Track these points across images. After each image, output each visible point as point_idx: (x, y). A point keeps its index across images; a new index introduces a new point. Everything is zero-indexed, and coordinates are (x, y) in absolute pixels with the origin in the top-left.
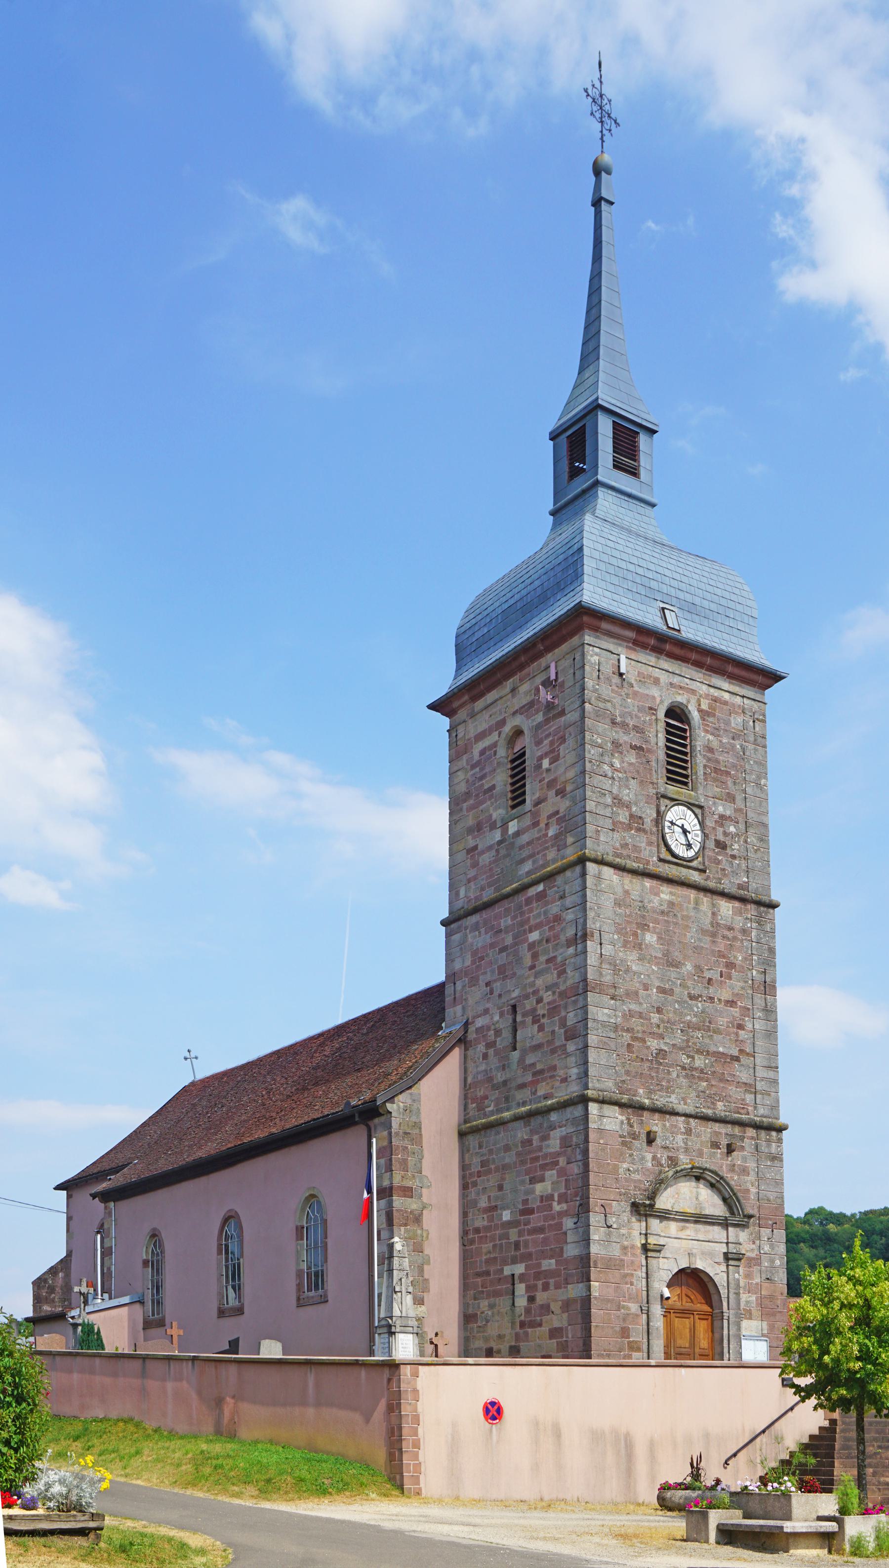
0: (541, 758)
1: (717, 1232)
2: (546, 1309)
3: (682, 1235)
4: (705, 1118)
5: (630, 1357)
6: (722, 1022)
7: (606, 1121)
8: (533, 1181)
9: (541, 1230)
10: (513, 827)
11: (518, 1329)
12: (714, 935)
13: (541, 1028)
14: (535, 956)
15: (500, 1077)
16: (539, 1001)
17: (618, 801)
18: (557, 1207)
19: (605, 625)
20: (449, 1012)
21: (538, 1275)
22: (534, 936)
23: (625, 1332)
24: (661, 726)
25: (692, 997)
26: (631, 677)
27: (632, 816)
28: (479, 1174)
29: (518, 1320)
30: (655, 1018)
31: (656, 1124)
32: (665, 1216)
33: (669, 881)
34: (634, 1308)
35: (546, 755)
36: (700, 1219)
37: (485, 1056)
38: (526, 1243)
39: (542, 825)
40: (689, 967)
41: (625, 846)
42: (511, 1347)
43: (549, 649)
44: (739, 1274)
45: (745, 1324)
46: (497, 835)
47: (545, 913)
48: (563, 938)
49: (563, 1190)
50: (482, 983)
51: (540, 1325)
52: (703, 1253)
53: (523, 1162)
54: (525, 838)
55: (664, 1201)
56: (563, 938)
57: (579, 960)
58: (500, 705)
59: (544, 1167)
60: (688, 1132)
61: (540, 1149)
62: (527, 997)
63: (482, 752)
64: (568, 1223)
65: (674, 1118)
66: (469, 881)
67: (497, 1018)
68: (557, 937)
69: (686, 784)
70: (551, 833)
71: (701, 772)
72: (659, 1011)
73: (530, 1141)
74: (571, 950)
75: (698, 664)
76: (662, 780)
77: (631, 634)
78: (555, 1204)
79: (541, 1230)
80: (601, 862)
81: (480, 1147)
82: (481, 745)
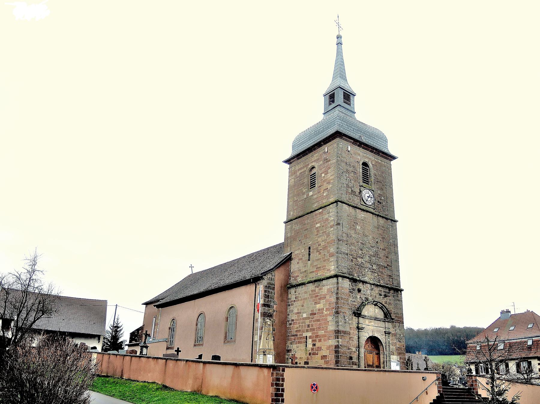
2: (320, 349)
3: (370, 324)
4: (377, 285)
5: (352, 367)
8: (316, 303)
9: (318, 320)
14: (318, 231)
15: (303, 270)
19: (344, 137)
22: (318, 225)
23: (351, 358)
26: (352, 152)
30: (360, 252)
31: (361, 286)
32: (364, 317)
34: (354, 349)
36: (376, 319)
37: (298, 263)
40: (371, 237)
42: (305, 362)
43: (325, 144)
45: (392, 356)
46: (305, 196)
48: (329, 226)
52: (377, 331)
54: (315, 196)
59: (320, 299)
60: (372, 289)
61: (319, 293)
62: (315, 244)
63: (300, 174)
68: (326, 225)
71: (373, 181)
73: (315, 290)
74: (332, 229)
78: (324, 311)
79: (318, 320)
82: (300, 172)
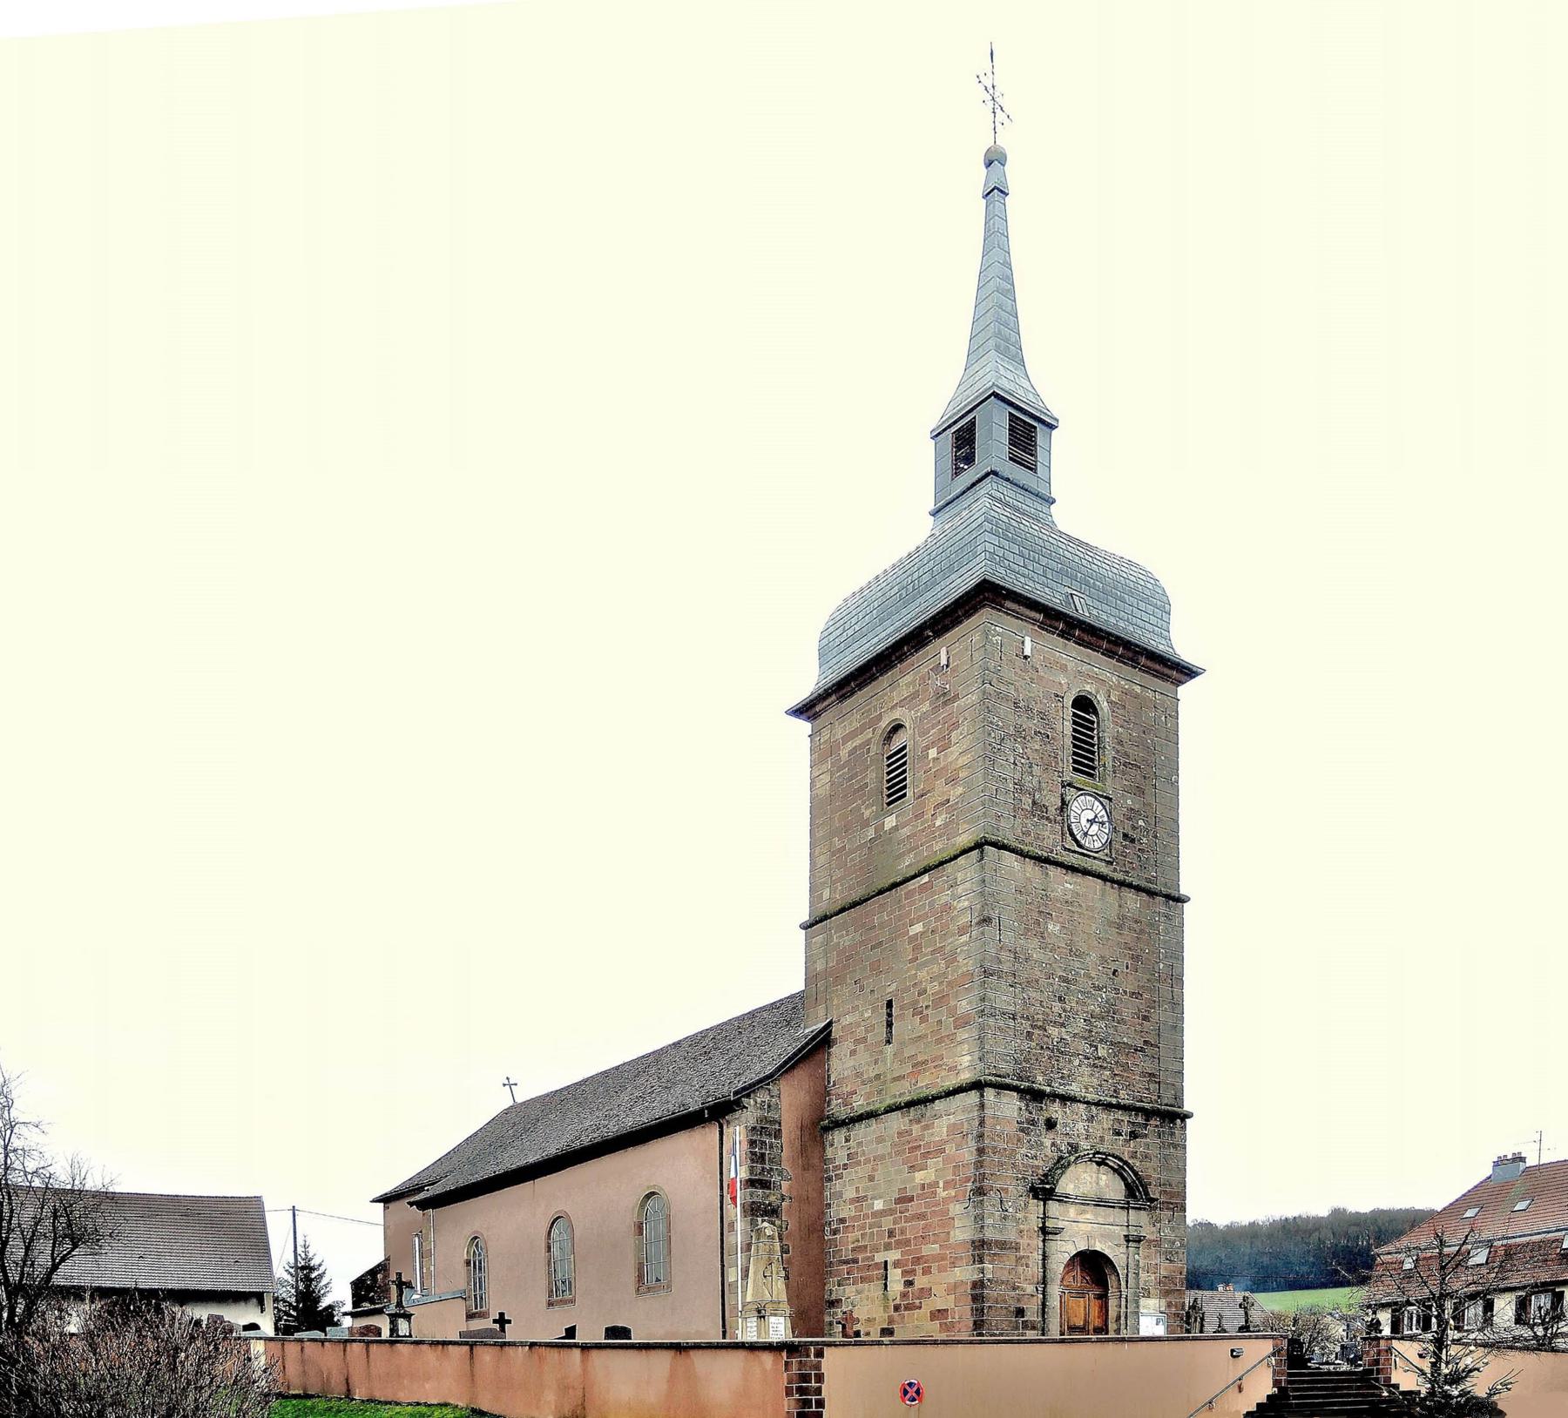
0: (927, 748)
1: (1119, 1216)
2: (926, 1292)
8: (913, 1168)
9: (922, 1216)
10: (890, 822)
12: (1120, 927)
13: (924, 1019)
14: (917, 948)
16: (922, 992)
21: (917, 1260)
22: (918, 928)
23: (1020, 1312)
24: (1070, 718)
26: (1037, 661)
27: (1034, 803)
28: (845, 1166)
29: (892, 1304)
30: (1057, 1007)
31: (1055, 1110)
32: (1063, 1199)
33: (1073, 869)
34: (1030, 1289)
36: (1100, 1203)
37: (853, 1053)
38: (903, 1232)
41: (1027, 833)
44: (1143, 1256)
45: (1143, 1301)
46: (871, 833)
47: (931, 904)
54: (906, 831)
55: (1066, 1185)
56: (953, 928)
60: (1091, 1119)
61: (921, 1138)
62: (907, 990)
65: (1075, 1105)
69: (1091, 775)
72: (1061, 999)
73: (909, 1132)
74: (965, 938)
76: (1068, 766)
79: (922, 1216)
81: (847, 1140)
82: (850, 745)
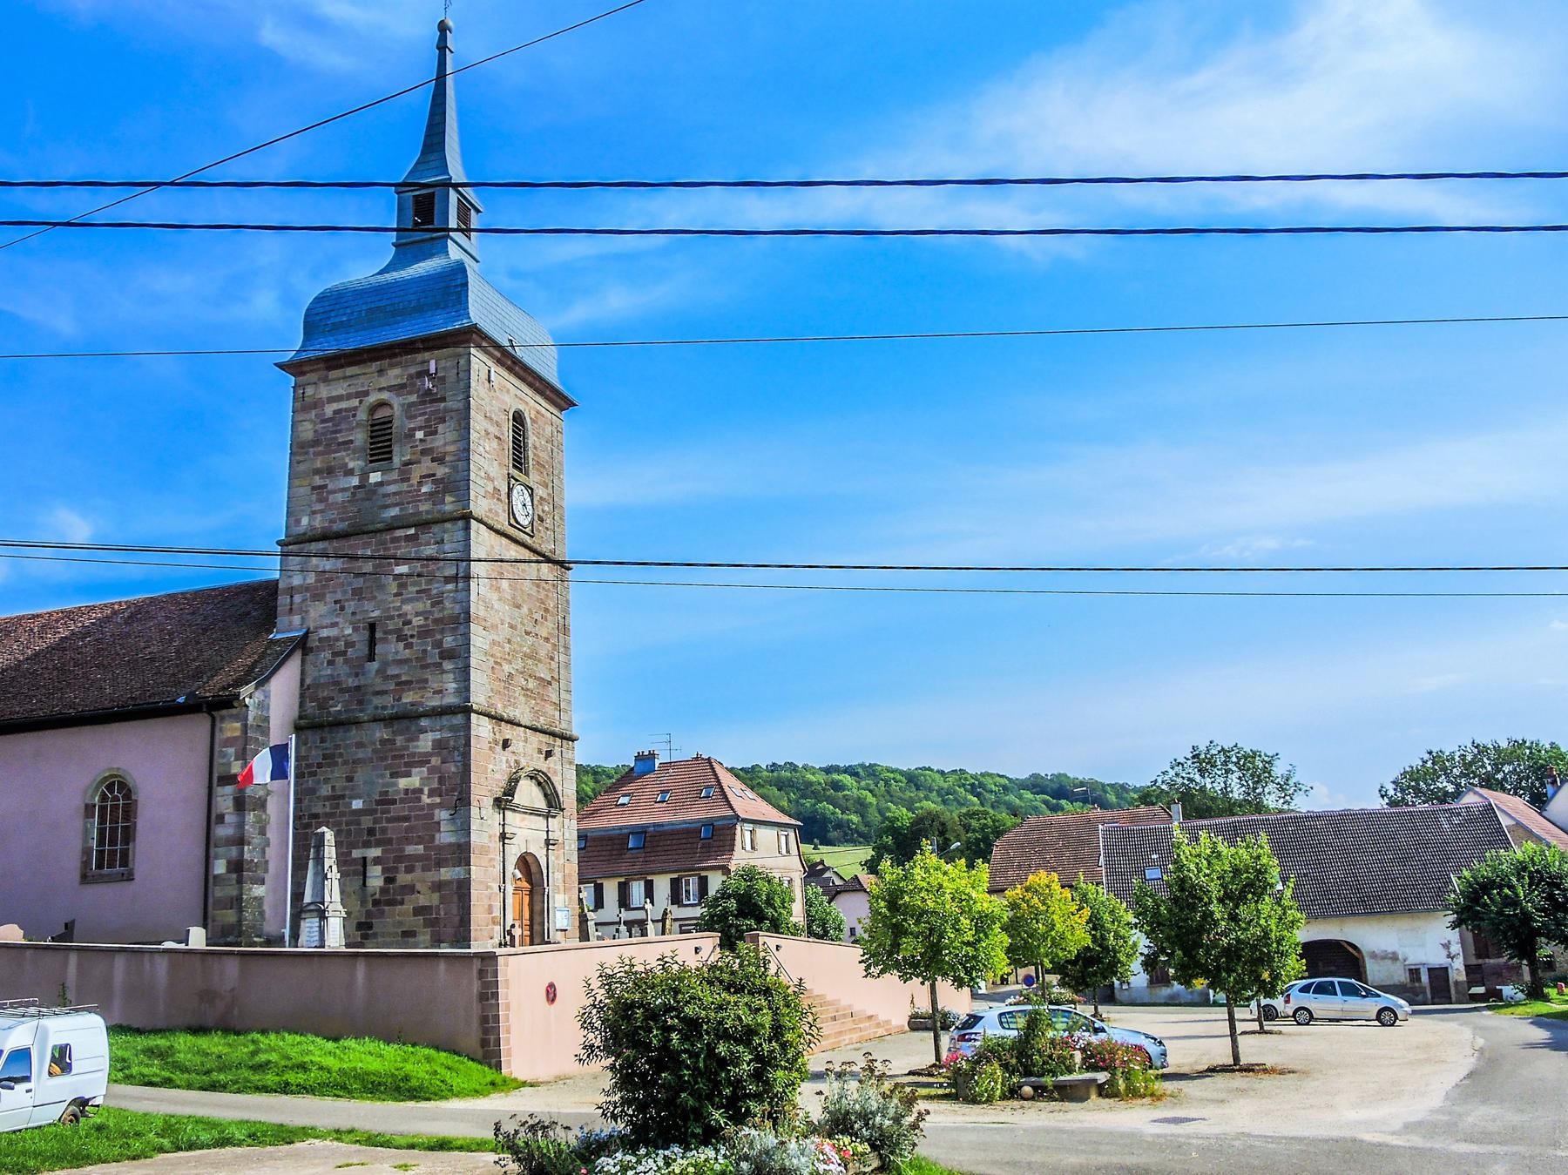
6: (542, 653)
7: (481, 729)
9: (406, 819)
11: (370, 906)
17: (488, 478)
18: (426, 800)
20: (282, 621)
25: (527, 633)
28: (320, 766)
31: (508, 732)
35: (420, 429)
37: (331, 663)
39: (414, 481)
46: (355, 481)
49: (436, 785)
50: (329, 598)
51: (402, 903)
53: (383, 759)
57: (460, 596)
58: (362, 379)
61: (407, 748)
63: (335, 412)
64: (443, 815)
66: (314, 513)
67: (349, 631)
70: (424, 490)
72: (509, 642)
73: (393, 742)
74: (450, 587)
75: (530, 385)
77: (498, 354)
79: (406, 819)
80: (480, 521)
82: (335, 406)
